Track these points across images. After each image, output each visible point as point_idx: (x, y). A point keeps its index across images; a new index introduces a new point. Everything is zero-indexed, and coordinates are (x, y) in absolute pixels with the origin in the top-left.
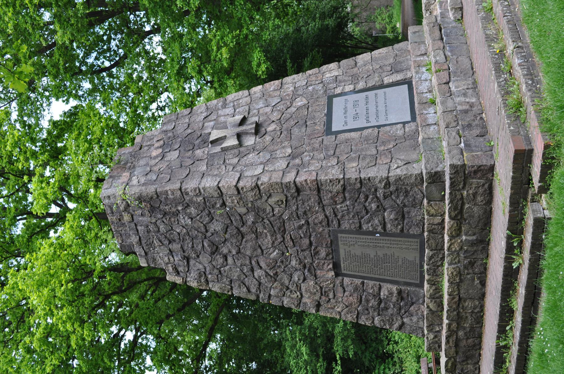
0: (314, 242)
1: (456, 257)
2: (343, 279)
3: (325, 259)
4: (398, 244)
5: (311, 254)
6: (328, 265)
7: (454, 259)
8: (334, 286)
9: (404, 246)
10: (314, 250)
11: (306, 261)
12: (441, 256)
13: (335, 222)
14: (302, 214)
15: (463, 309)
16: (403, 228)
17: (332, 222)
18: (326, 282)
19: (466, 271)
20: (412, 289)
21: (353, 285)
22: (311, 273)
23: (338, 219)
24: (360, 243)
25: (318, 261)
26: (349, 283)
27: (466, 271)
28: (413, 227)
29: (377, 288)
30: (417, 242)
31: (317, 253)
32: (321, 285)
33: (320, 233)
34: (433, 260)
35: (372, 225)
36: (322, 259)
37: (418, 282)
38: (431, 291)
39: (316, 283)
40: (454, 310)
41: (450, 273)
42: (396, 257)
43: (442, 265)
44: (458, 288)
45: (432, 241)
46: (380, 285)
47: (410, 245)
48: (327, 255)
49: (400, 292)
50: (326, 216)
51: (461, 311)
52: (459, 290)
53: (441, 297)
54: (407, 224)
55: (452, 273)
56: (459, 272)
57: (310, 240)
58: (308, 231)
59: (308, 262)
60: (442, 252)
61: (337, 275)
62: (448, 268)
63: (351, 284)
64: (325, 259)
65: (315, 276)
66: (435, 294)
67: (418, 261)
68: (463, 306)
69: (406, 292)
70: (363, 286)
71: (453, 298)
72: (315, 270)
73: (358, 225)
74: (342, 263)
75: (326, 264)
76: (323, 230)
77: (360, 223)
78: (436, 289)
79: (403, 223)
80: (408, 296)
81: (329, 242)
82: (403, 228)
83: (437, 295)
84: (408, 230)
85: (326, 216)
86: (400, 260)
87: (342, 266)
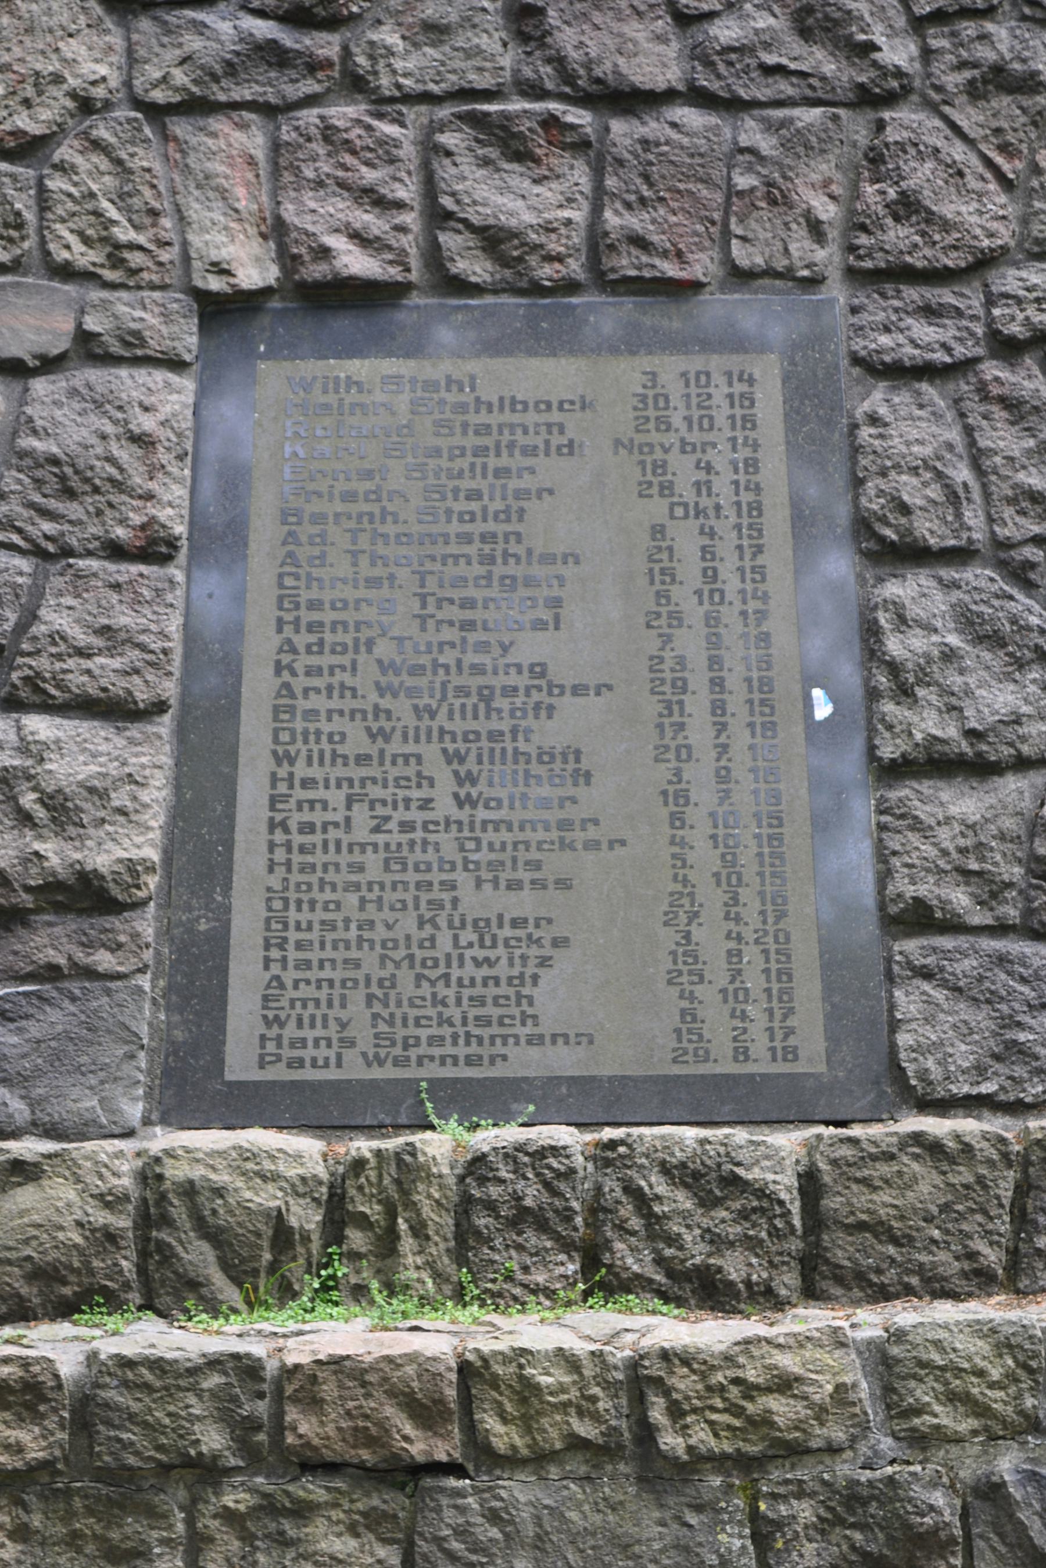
0: (652, 127)
1: (980, 1409)
2: (177, 365)
3: (438, 217)
4: (729, 877)
5: (488, 95)
6: (360, 238)
7: (952, 1398)
8: (66, 272)
9: (710, 939)
10: (550, 122)
11: (390, 37)
12: (735, 1267)
13: (925, 332)
14: (985, 54)
15: (268, 1507)
16: (954, 926)
17: (930, 312)
18: (121, 198)
19: (805, 1511)
20: (146, 1011)
21: (124, 453)
22: (231, 69)
23: (968, 365)
24: (686, 540)
25: (408, 151)
26: (147, 423)
27: (805, 1511)
28: (981, 1018)
29: (118, 686)
30: (791, 1054)
31: (508, 144)
32: (65, 152)
33: (777, 197)
34: (684, 1201)
35: (949, 655)
36: (430, 187)
37: (240, 1063)
38: (267, 1198)
39: (86, 106)
40: (243, 1430)
41: (788, 1362)
42: (556, 864)
43: (603, 1282)
44: (576, 1444)
45: (927, 1184)
46: (160, 707)
47: (735, 995)
48: (493, 239)
49: (88, 896)
50: (985, 262)
51: (235, 1498)
52: (539, 1460)
53: (165, 1290)
54: (1002, 960)
55: (784, 1384)
56: (794, 1451)
57: (670, 96)
58: (786, 88)
59: (377, 52)
60: (788, 1281)
61: (224, 311)
62: (838, 1340)
63: (142, 440)
64: (438, 217)
65: (196, 106)
66: (214, 1236)
67: (524, 1062)
68: (302, 1511)
69: (104, 960)
70: (116, 551)
71: (426, 1412)
72: (269, 111)
73: (930, 530)
74: (390, 366)
75: (367, 219)
76: (816, 229)
77: (961, 555)
78: (283, 1236)
79: (1001, 929)
80: (51, 973)
81: (670, 269)
82: (954, 926)
83: (198, 1256)
84: (926, 974)
85: (985, 262)
86: (525, 903)
87: (357, 367)
